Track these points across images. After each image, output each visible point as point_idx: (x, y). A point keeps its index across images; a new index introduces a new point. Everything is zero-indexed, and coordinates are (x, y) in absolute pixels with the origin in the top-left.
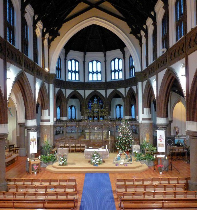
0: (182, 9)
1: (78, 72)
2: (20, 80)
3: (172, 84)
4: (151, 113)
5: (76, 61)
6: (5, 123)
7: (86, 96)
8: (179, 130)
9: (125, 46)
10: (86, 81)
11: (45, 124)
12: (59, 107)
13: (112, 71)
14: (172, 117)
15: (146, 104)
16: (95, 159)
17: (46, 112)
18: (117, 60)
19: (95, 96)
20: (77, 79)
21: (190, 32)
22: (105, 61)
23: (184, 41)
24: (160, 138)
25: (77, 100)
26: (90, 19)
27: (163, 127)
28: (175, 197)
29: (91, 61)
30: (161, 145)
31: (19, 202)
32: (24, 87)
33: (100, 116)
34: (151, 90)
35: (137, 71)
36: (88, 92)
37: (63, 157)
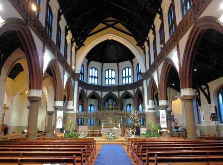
0: (173, 16)
1: (97, 78)
2: (53, 66)
4: (154, 104)
5: (95, 69)
6: (40, 89)
7: (103, 96)
8: (177, 121)
10: (103, 85)
11: (70, 112)
12: (81, 105)
13: (123, 78)
15: (150, 97)
16: (110, 135)
17: (71, 102)
19: (110, 97)
20: (96, 83)
22: (118, 70)
23: (175, 34)
24: (162, 116)
25: (96, 100)
26: (106, 35)
29: (107, 70)
30: (163, 122)
32: (56, 73)
34: (154, 83)
35: (143, 72)
36: (105, 93)
37: (84, 133)
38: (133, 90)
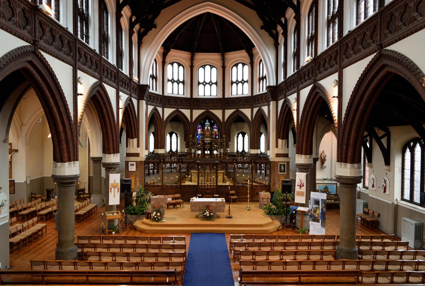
1: (183, 82)
3: (318, 104)
5: (179, 65)
9: (254, 46)
13: (232, 83)
14: (317, 153)
18: (240, 66)
20: (181, 92)
21: (347, 36)
24: (300, 184)
27: (304, 169)
28: (314, 268)
29: (202, 67)
31: (82, 276)
33: (213, 148)
38: (250, 110)
